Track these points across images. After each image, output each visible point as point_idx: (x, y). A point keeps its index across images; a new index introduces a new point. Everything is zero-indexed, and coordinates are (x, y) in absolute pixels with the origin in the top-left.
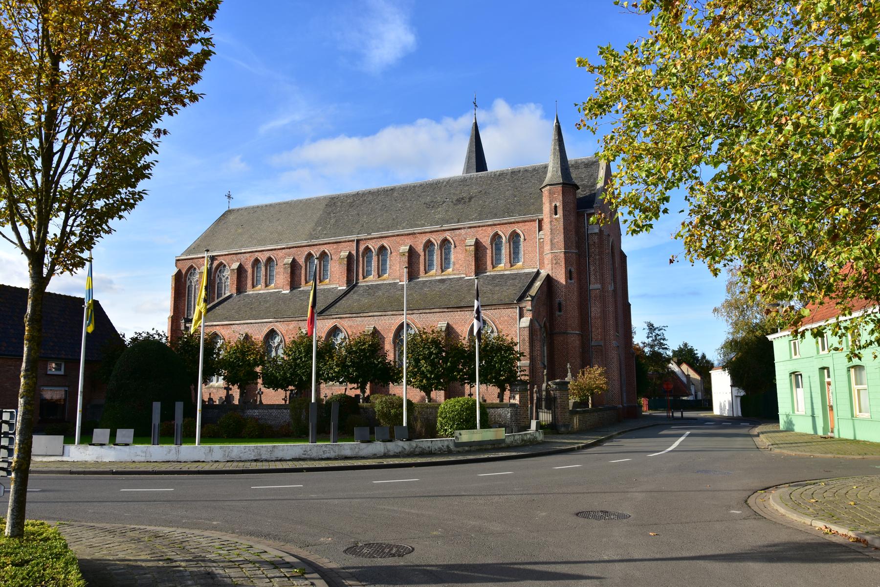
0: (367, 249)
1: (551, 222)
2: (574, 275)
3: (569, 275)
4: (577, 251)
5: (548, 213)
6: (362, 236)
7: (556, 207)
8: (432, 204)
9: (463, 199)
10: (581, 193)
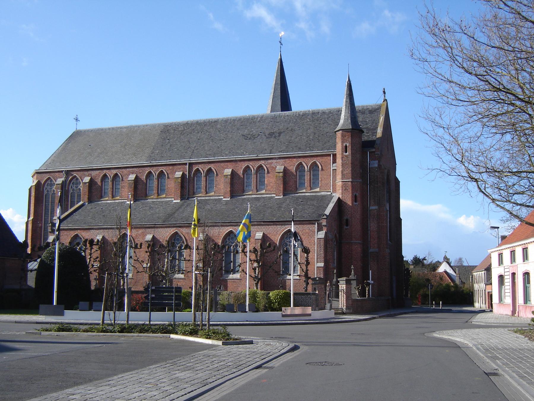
0: (198, 170)
1: (342, 158)
2: (359, 199)
3: (355, 199)
4: (361, 180)
5: (341, 151)
6: (193, 160)
7: (346, 147)
8: (249, 136)
9: (273, 133)
10: (365, 138)
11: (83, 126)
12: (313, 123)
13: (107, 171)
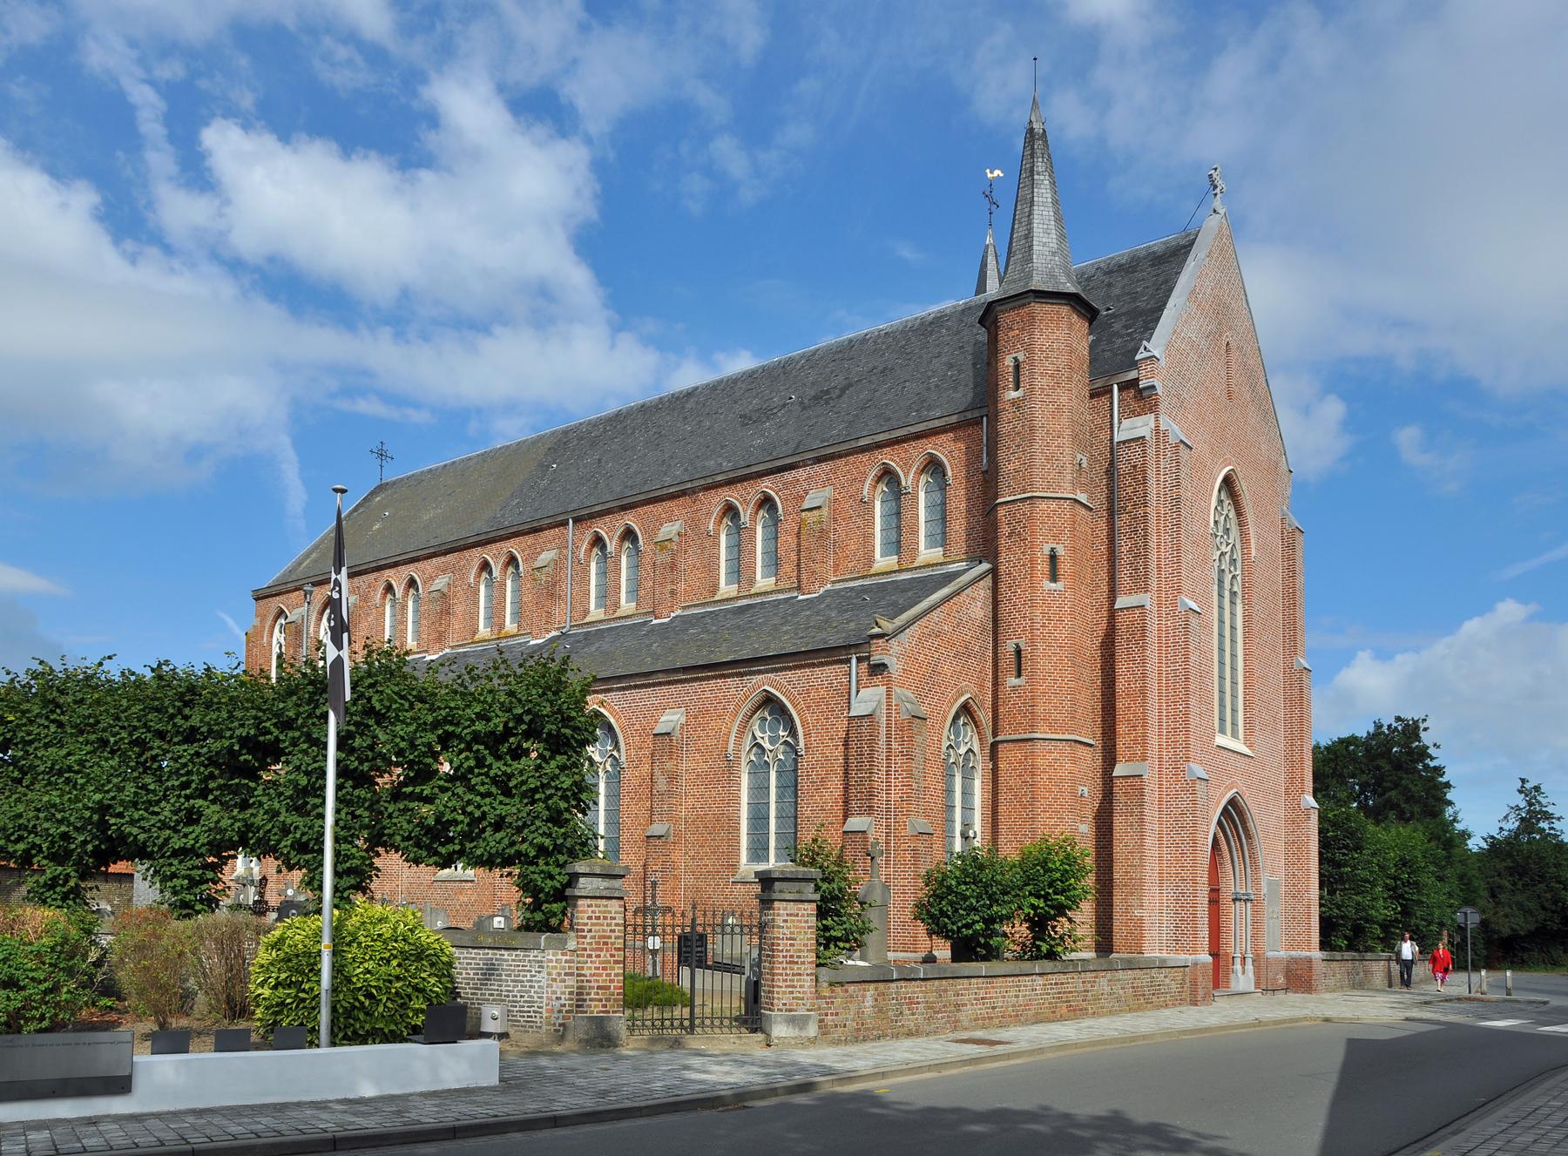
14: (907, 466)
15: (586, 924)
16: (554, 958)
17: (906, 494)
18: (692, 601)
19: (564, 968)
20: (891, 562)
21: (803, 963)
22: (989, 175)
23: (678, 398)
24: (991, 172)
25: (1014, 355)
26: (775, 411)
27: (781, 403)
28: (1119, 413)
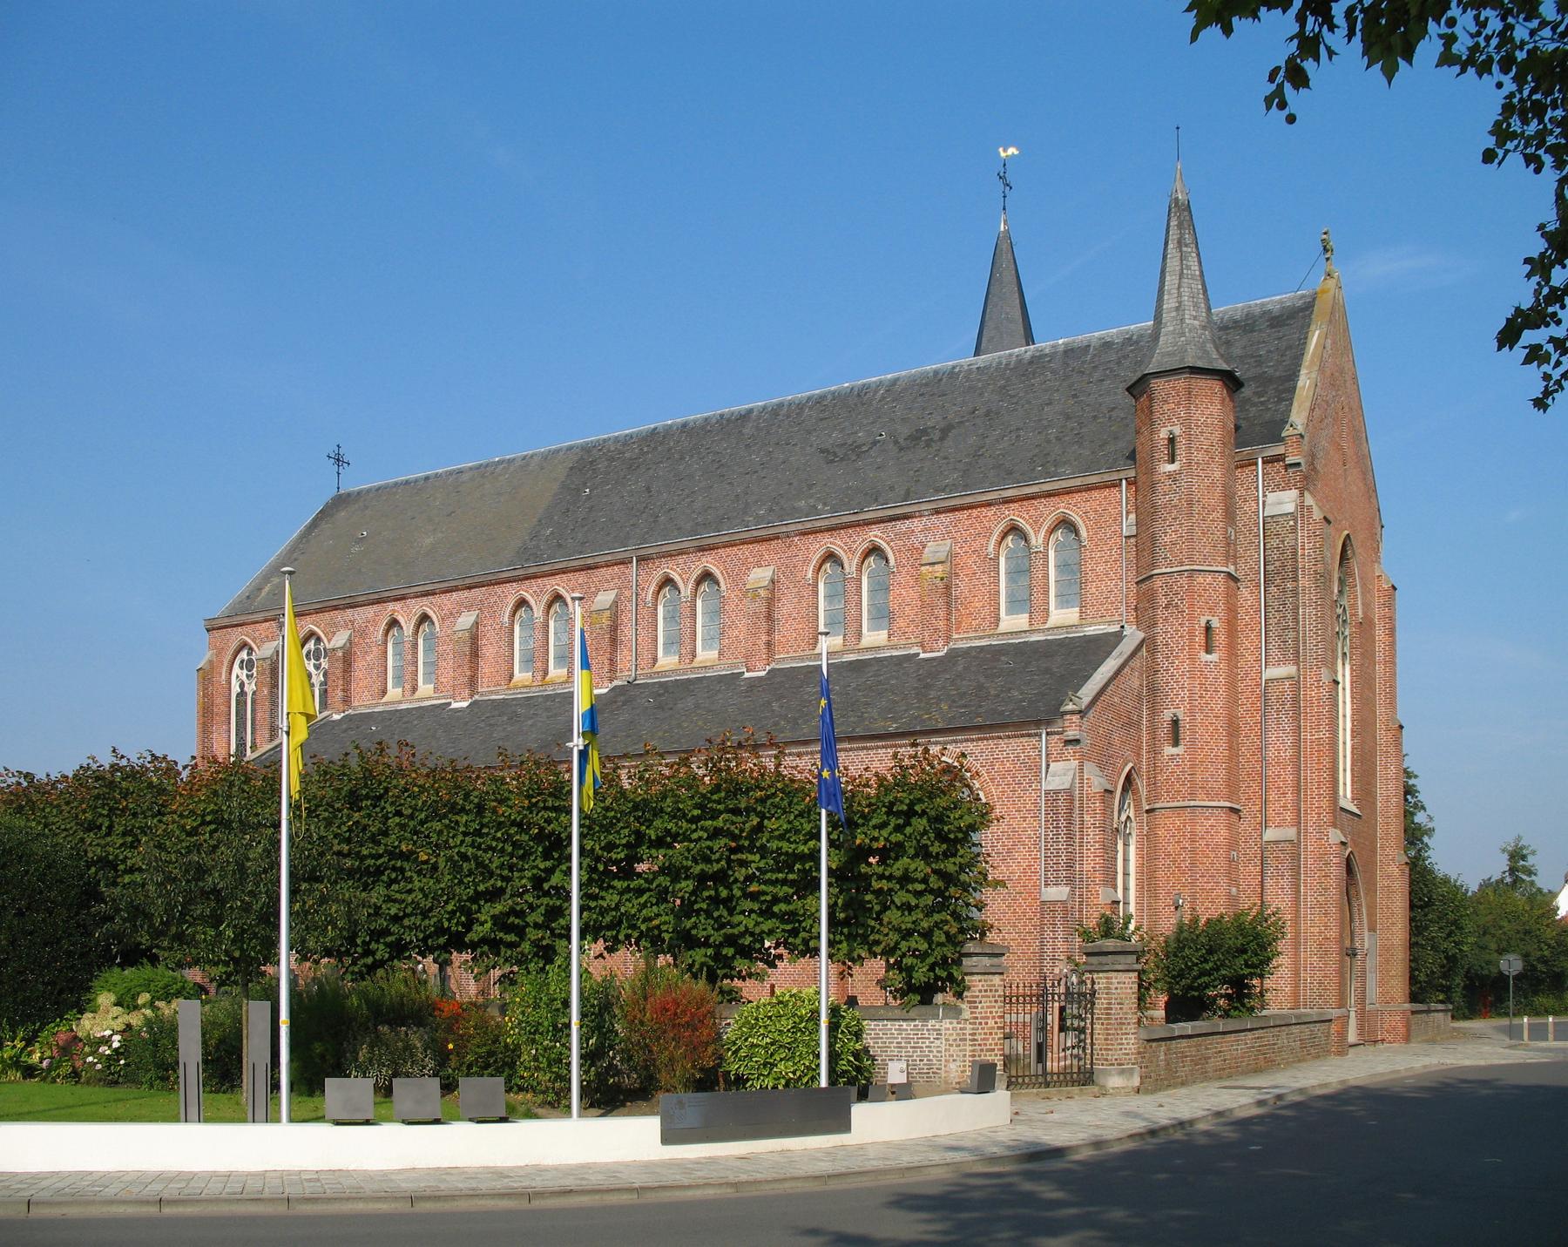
8: (840, 453)
9: (924, 432)
11: (354, 482)
12: (1065, 384)
13: (397, 606)
14: (1036, 524)
15: (978, 997)
16: (951, 1027)
17: (1036, 552)
18: (788, 653)
19: (958, 1034)
20: (1021, 621)
21: (1129, 1024)
22: (1003, 154)
23: (728, 420)
24: (1005, 151)
25: (1170, 428)
26: (865, 448)
27: (871, 440)
28: (1264, 486)
